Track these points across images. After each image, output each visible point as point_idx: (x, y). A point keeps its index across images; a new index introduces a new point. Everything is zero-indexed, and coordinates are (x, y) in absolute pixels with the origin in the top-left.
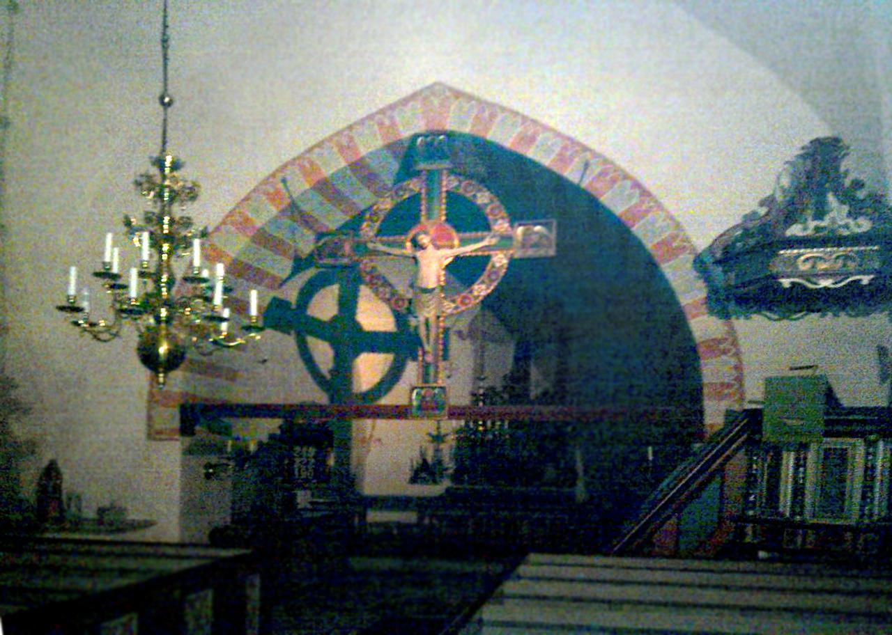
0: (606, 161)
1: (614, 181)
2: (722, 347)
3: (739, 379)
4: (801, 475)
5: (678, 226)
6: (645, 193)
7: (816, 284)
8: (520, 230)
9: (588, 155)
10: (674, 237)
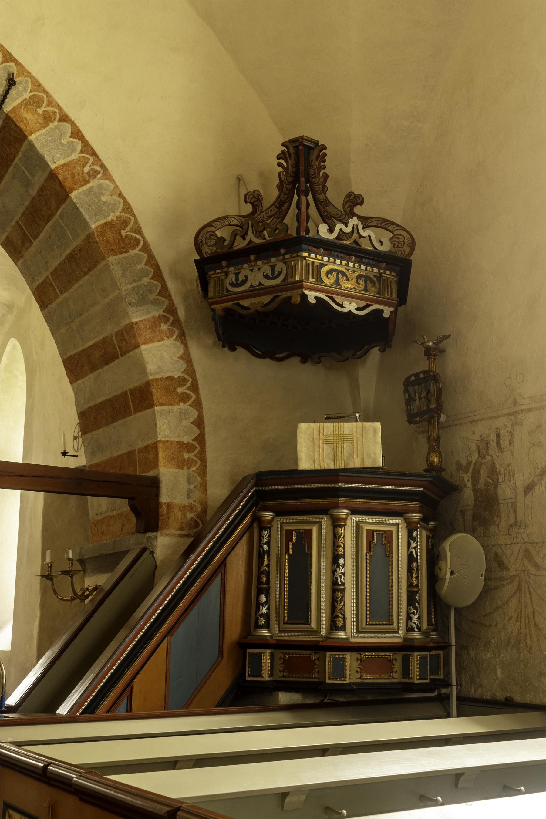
0: (37, 85)
1: (47, 119)
2: (180, 390)
3: (201, 439)
4: (265, 539)
5: (128, 208)
6: (87, 148)
7: (341, 306)
8: (388, 272)
9: (14, 69)
10: (125, 223)
